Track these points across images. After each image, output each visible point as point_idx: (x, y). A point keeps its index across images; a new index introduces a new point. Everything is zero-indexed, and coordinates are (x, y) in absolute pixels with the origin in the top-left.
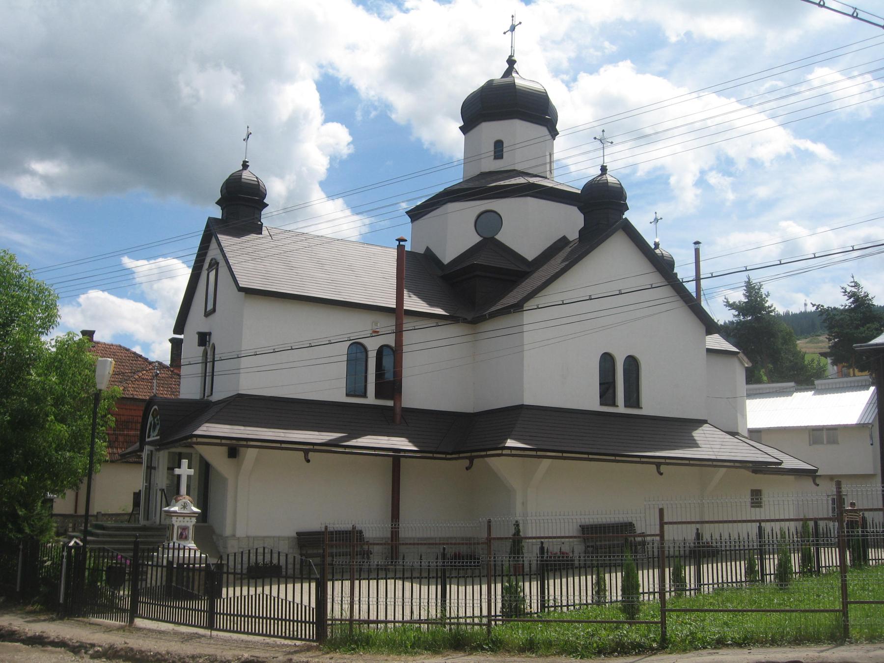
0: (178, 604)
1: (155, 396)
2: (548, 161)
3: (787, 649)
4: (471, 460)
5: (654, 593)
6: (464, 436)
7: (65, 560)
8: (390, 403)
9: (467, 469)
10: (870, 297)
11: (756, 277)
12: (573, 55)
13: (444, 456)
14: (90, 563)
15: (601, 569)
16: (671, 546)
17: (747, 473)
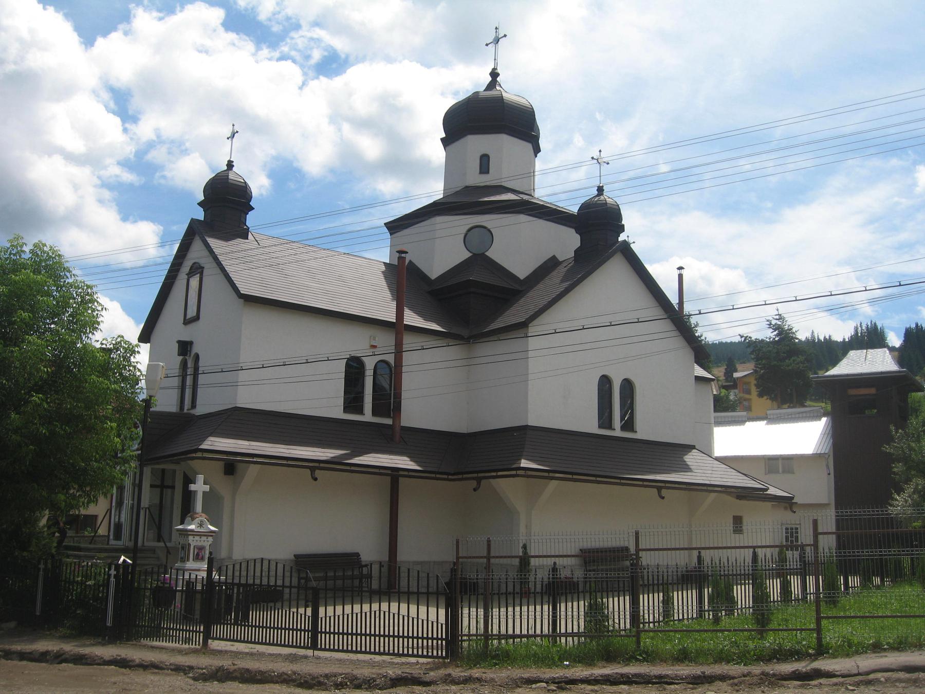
3: (909, 653)
4: (479, 480)
5: (442, 639)
6: (473, 458)
8: (389, 421)
9: (475, 490)
10: (794, 330)
11: (783, 309)
16: (665, 570)
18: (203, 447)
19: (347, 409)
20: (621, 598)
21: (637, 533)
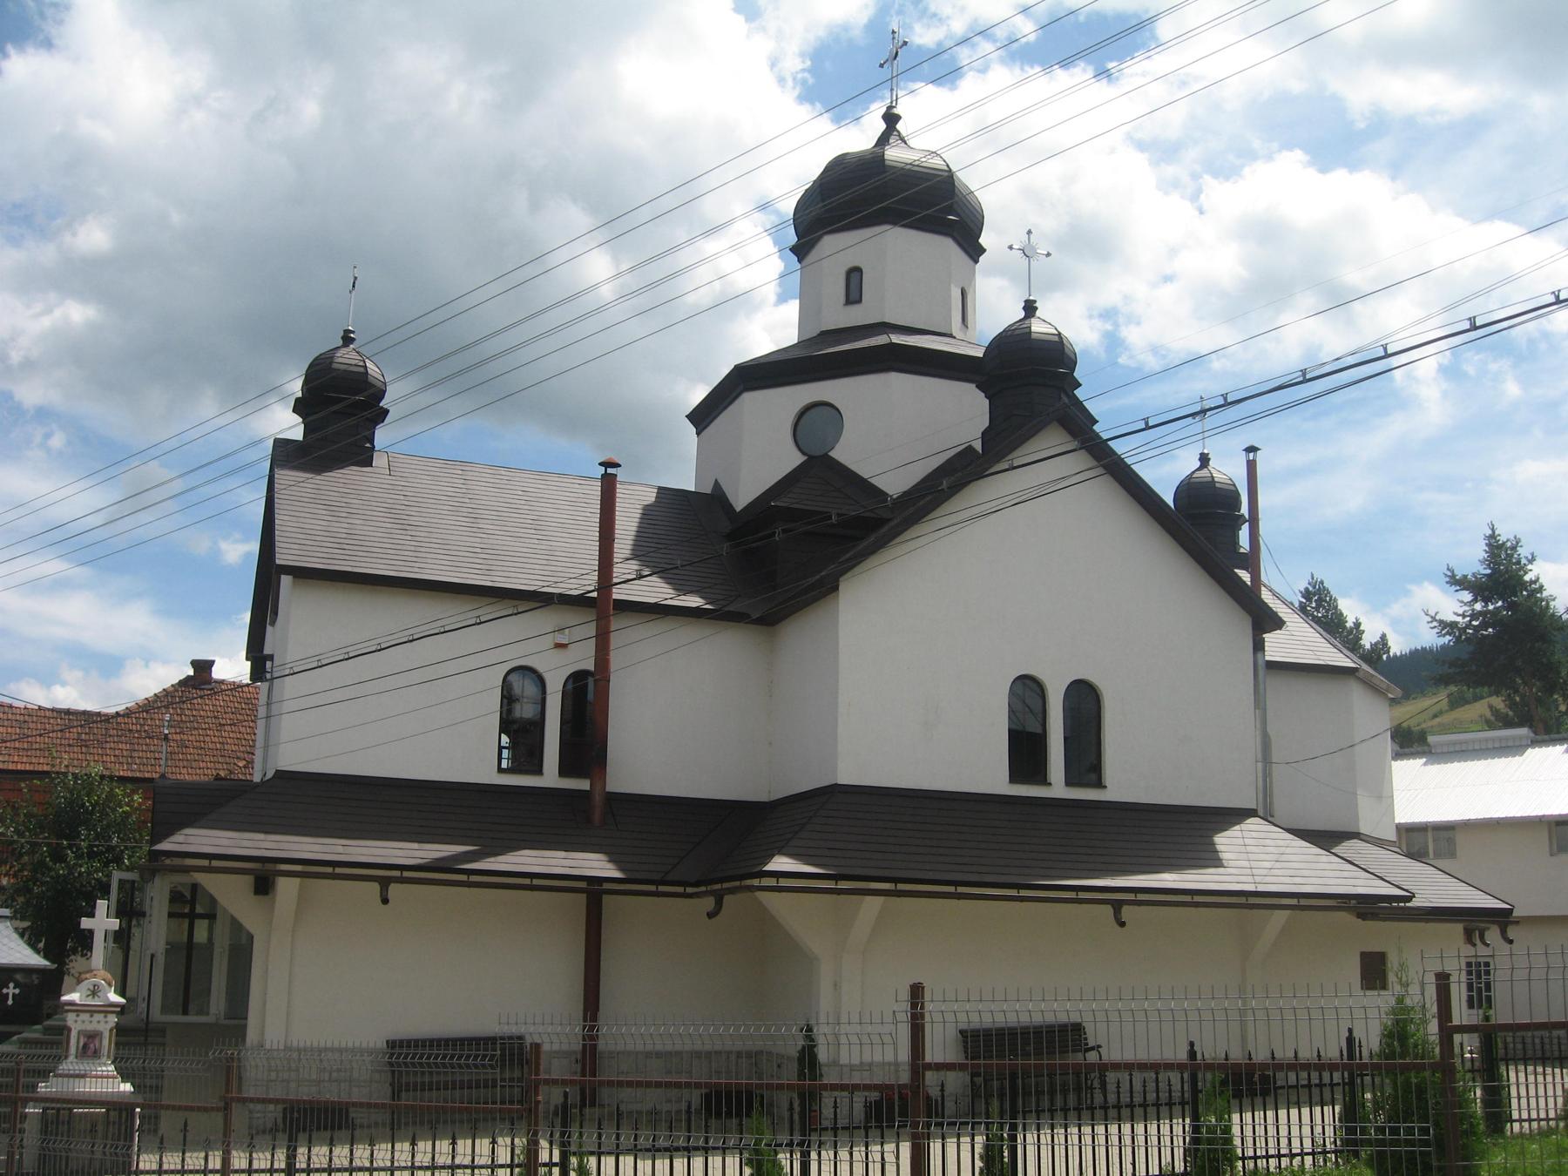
6: (706, 846)
8: (584, 785)
9: (710, 915)
17: (1346, 918)
19: (1016, 775)
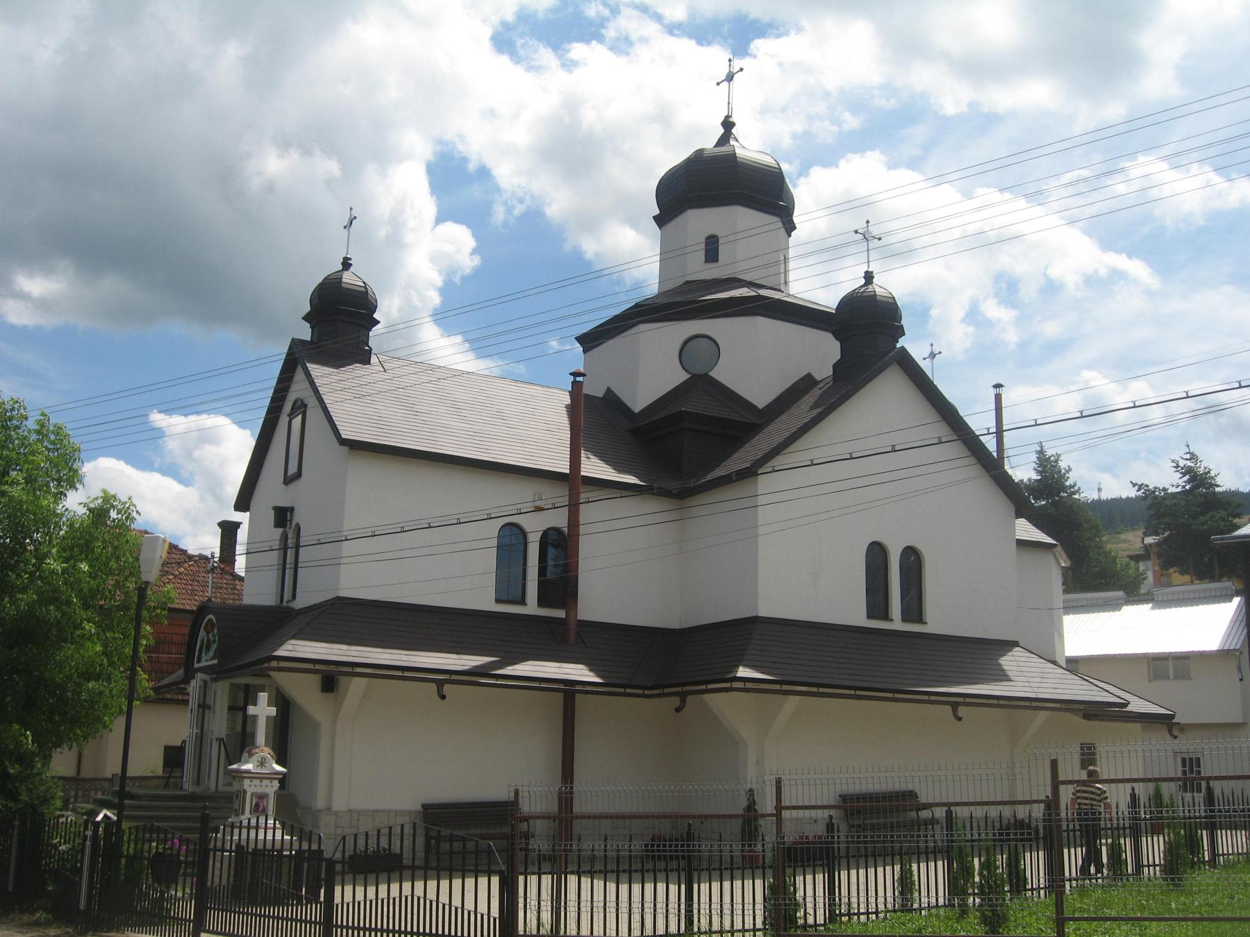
0: (271, 911)
1: (210, 599)
2: (782, 270)
4: (683, 696)
6: (672, 663)
7: (88, 843)
8: (561, 614)
9: (677, 710)
10: (1212, 473)
12: (799, 128)
13: (640, 691)
14: (129, 848)
15: (906, 858)
18: (279, 653)
20: (932, 864)
21: (779, 782)
